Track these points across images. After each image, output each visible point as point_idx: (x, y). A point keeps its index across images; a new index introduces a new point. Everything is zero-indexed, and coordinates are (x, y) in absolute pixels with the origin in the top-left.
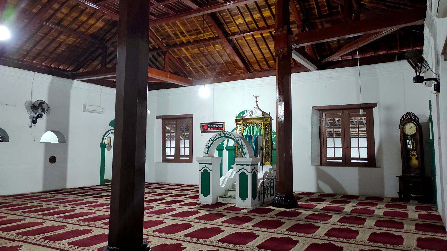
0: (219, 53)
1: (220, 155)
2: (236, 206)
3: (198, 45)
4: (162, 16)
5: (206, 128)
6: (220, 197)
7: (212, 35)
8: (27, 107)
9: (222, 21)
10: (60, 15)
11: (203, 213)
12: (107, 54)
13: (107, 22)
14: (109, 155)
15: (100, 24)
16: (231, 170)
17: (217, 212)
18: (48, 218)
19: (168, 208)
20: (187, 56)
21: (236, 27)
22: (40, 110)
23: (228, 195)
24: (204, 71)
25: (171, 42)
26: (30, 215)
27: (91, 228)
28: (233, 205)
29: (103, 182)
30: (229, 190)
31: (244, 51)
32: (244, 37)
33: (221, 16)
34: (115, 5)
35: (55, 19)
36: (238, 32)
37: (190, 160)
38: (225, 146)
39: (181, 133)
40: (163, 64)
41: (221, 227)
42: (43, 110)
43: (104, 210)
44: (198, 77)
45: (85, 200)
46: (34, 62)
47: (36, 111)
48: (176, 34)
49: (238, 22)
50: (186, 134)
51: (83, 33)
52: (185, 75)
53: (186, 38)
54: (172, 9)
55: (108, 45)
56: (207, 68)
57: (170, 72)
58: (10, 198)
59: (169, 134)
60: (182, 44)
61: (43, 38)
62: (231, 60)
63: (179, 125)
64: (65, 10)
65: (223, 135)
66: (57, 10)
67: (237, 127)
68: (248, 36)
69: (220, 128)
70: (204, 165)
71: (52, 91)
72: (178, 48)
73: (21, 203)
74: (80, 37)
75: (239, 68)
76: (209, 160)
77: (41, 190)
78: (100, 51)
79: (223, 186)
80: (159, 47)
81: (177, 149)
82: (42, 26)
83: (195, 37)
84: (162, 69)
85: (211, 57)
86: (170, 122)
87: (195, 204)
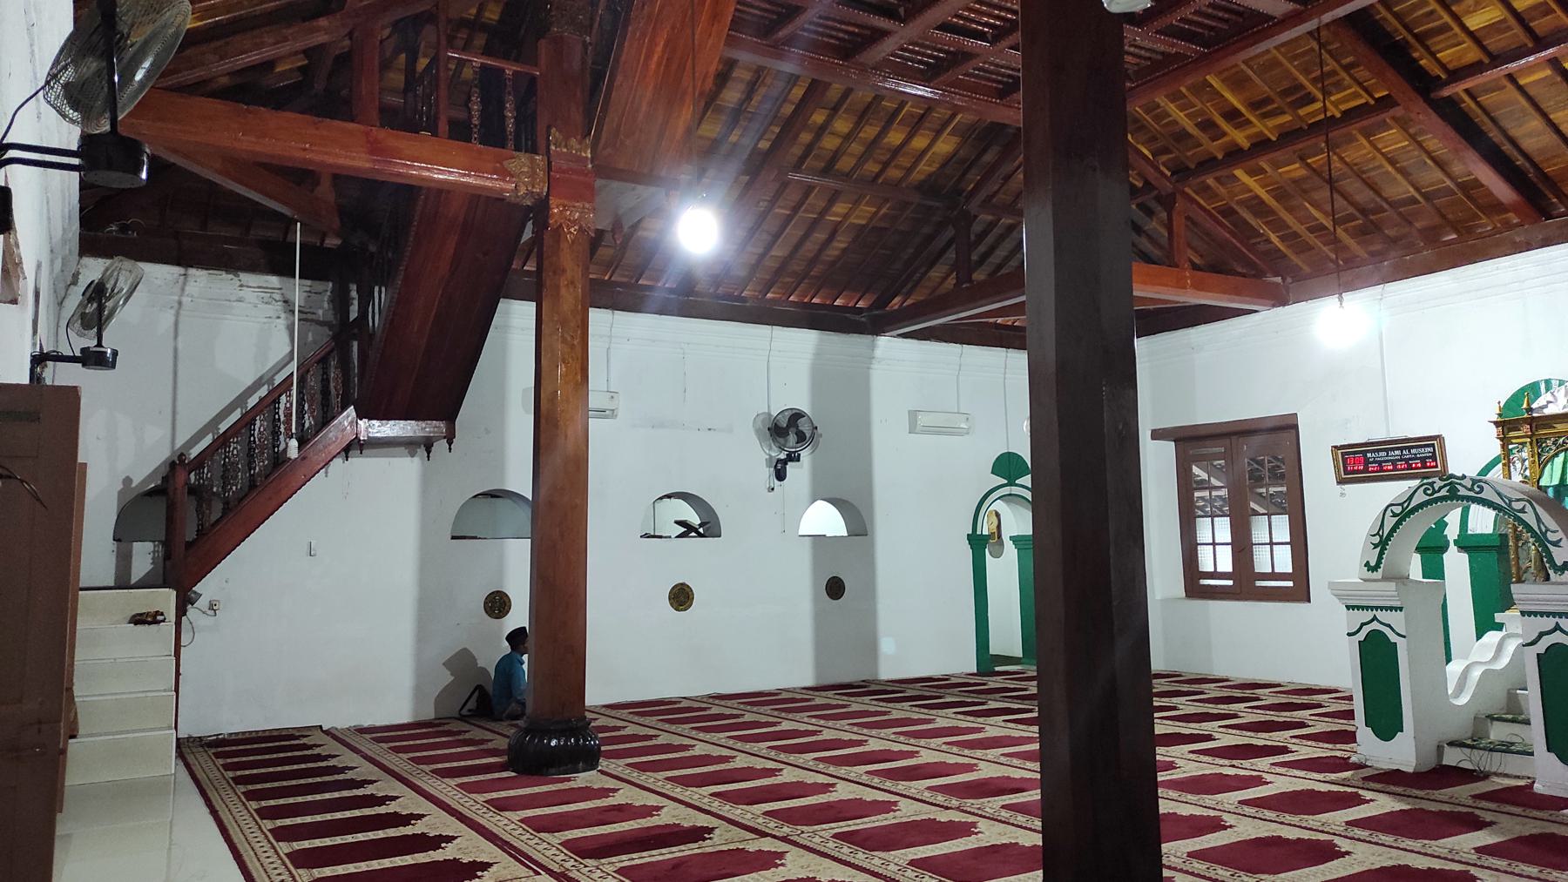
0: (1392, 162)
1: (1434, 569)
2: (1538, 788)
3: (1300, 146)
4: (1162, 69)
5: (1358, 463)
6: (1451, 744)
7: (1360, 96)
8: (758, 432)
9: (1402, 34)
10: (830, 143)
11: (1382, 804)
12: (973, 237)
13: (965, 133)
14: (1005, 572)
15: (945, 146)
16: (1492, 637)
17: (1447, 808)
18: (792, 758)
19: (1232, 771)
20: (1257, 197)
21: (1468, 43)
22: (792, 438)
23: (1493, 737)
24: (1335, 241)
25: (1191, 156)
26: (748, 747)
27: (971, 819)
28: (1521, 783)
29: (988, 662)
30: (1491, 718)
31: (1515, 132)
32: (1511, 78)
33: (1396, 16)
34: (992, 73)
35: (817, 157)
36: (1480, 62)
37: (1298, 588)
38: (1452, 532)
39: (1252, 488)
40: (1164, 241)
41: (1337, 840)
42: (801, 438)
43: (944, 747)
44: (1307, 269)
45: (941, 723)
46: (769, 295)
47: (781, 440)
48: (1207, 126)
49: (1475, 22)
50: (1272, 490)
51: (896, 185)
52: (1259, 266)
53: (1253, 130)
54: (1190, 37)
55: (973, 206)
56: (1346, 230)
57: (1195, 267)
58: (734, 703)
59: (1206, 494)
60: (1235, 155)
61: (789, 219)
62: (1417, 189)
63: (1253, 461)
64: (842, 125)
65: (1444, 492)
66: (821, 130)
67: (1507, 453)
68: (1530, 69)
69: (1423, 460)
70: (1369, 615)
71: (820, 378)
72: (1218, 174)
73: (728, 712)
74: (887, 200)
75: (1496, 207)
76: (1386, 592)
77: (810, 683)
78: (950, 232)
79: (1463, 700)
80: (1147, 182)
81: (1242, 547)
82: (785, 185)
83: (1287, 118)
84: (1164, 259)
85: (1358, 185)
86: (1204, 451)
87: (1342, 764)
